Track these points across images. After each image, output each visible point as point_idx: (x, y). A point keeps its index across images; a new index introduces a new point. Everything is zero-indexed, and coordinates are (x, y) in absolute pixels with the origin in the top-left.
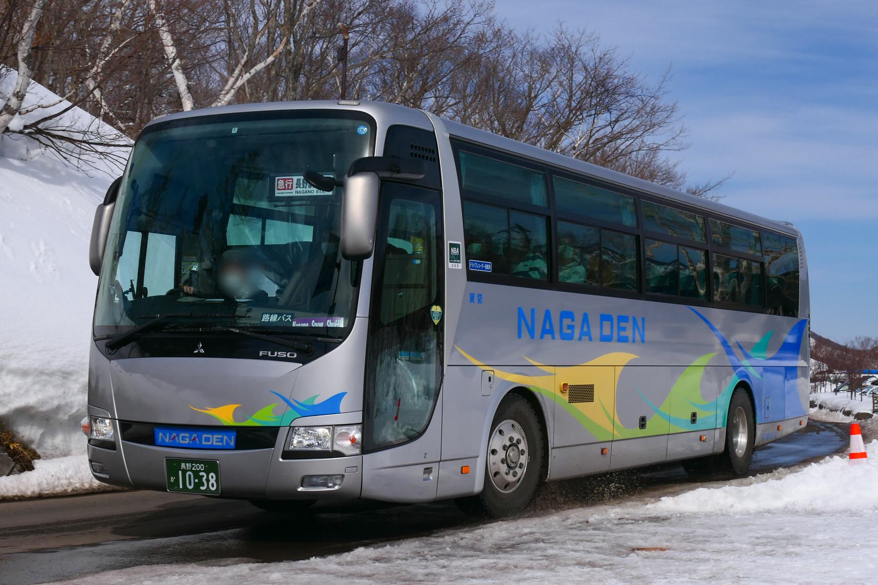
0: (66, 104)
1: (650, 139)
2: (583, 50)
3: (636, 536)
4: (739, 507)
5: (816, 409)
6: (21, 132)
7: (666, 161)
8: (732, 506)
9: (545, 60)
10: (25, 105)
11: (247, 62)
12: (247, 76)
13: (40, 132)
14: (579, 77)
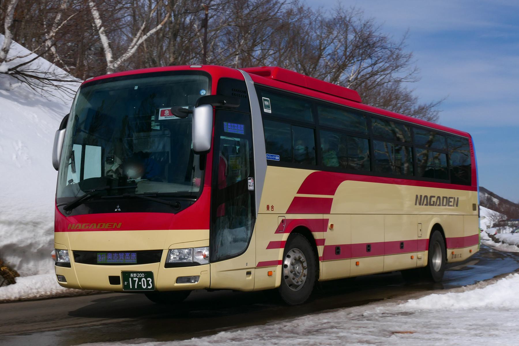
0: (35, 55)
1: (395, 75)
2: (354, 19)
3: (394, 324)
4: (457, 306)
5: (500, 244)
6: (6, 73)
7: (405, 89)
8: (453, 305)
9: (330, 26)
10: (9, 56)
11: (144, 28)
12: (145, 37)
13: (18, 73)
14: (351, 37)
